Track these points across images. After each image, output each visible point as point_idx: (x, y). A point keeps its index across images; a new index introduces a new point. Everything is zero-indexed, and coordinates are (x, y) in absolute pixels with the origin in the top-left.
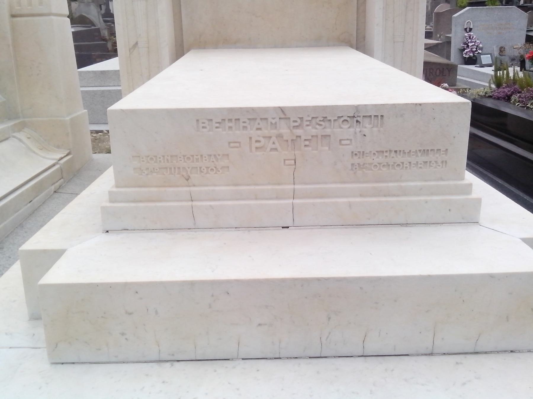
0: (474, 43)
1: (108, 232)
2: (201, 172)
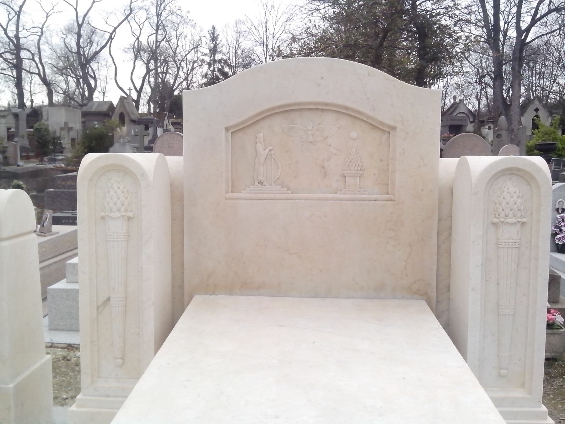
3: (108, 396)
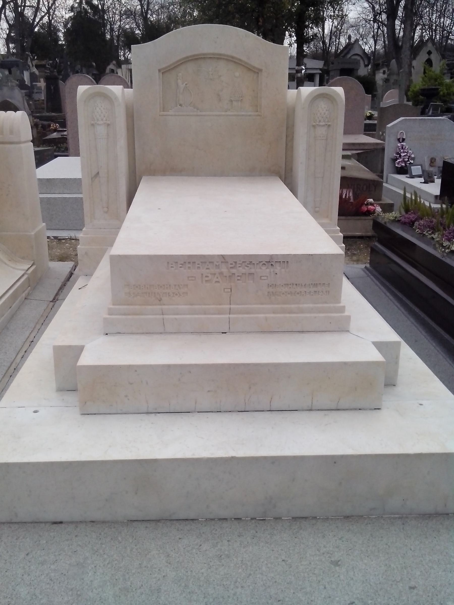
0: (406, 153)
1: (107, 334)
2: (169, 296)
3: (101, 229)
